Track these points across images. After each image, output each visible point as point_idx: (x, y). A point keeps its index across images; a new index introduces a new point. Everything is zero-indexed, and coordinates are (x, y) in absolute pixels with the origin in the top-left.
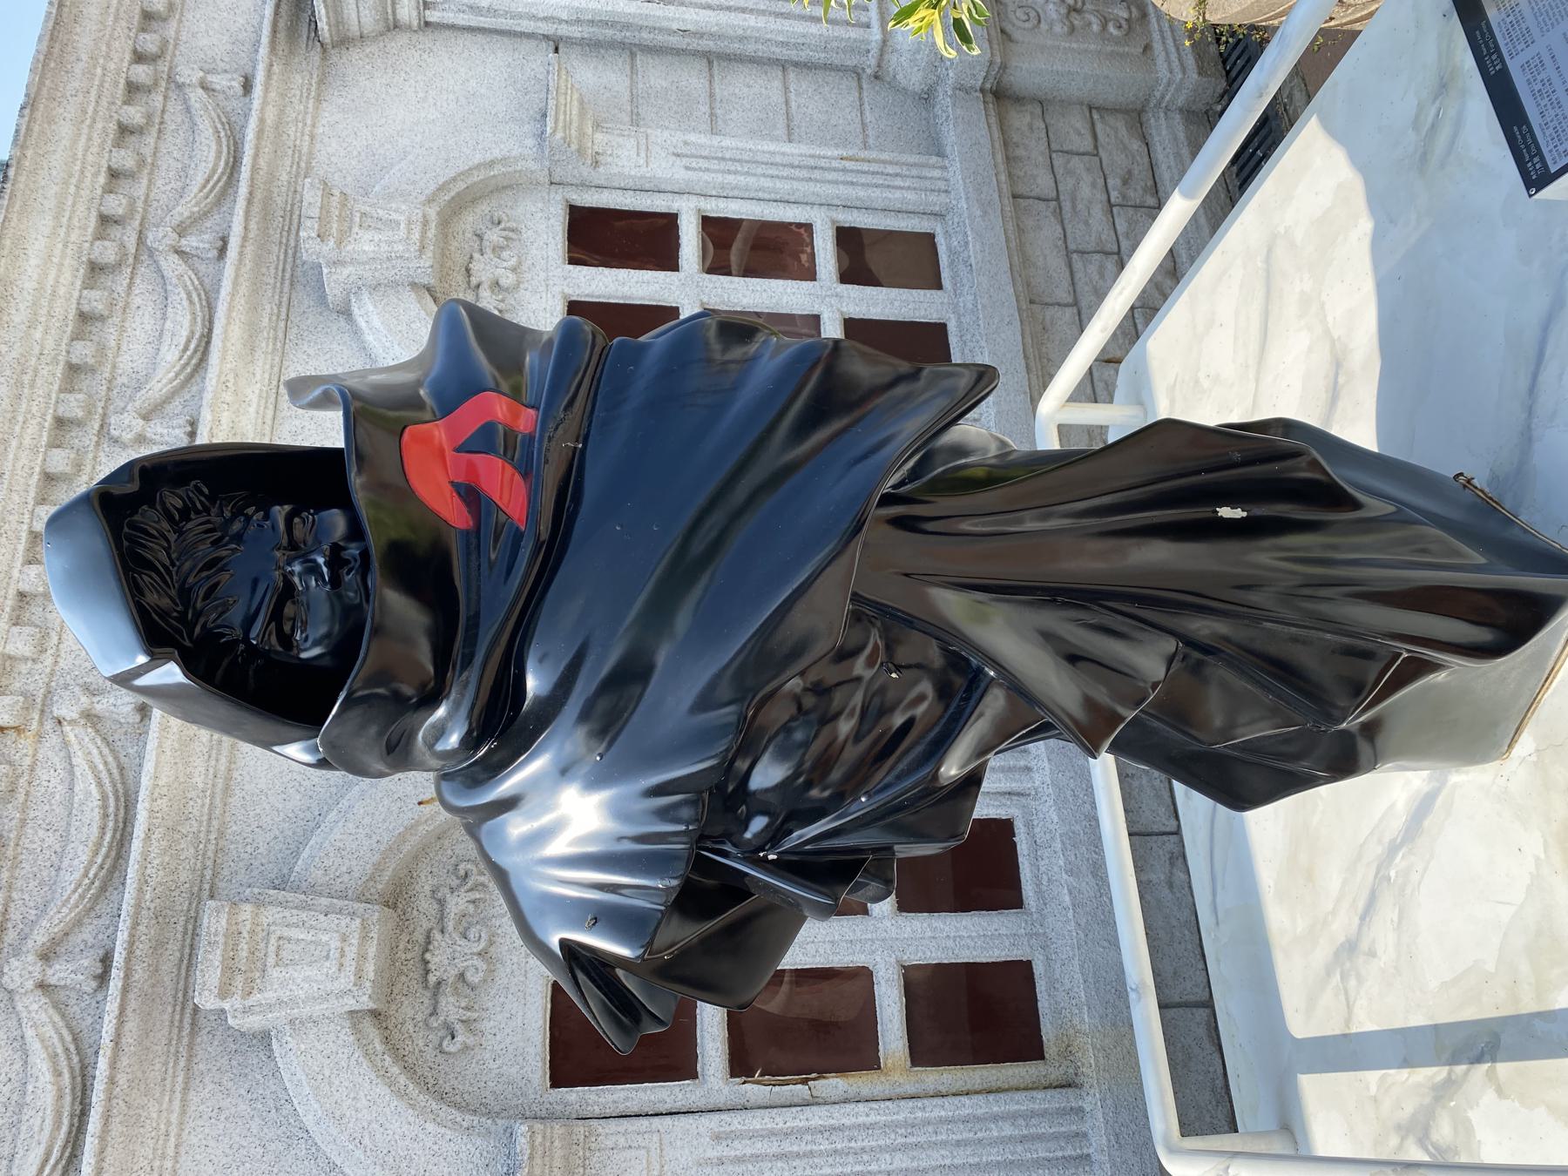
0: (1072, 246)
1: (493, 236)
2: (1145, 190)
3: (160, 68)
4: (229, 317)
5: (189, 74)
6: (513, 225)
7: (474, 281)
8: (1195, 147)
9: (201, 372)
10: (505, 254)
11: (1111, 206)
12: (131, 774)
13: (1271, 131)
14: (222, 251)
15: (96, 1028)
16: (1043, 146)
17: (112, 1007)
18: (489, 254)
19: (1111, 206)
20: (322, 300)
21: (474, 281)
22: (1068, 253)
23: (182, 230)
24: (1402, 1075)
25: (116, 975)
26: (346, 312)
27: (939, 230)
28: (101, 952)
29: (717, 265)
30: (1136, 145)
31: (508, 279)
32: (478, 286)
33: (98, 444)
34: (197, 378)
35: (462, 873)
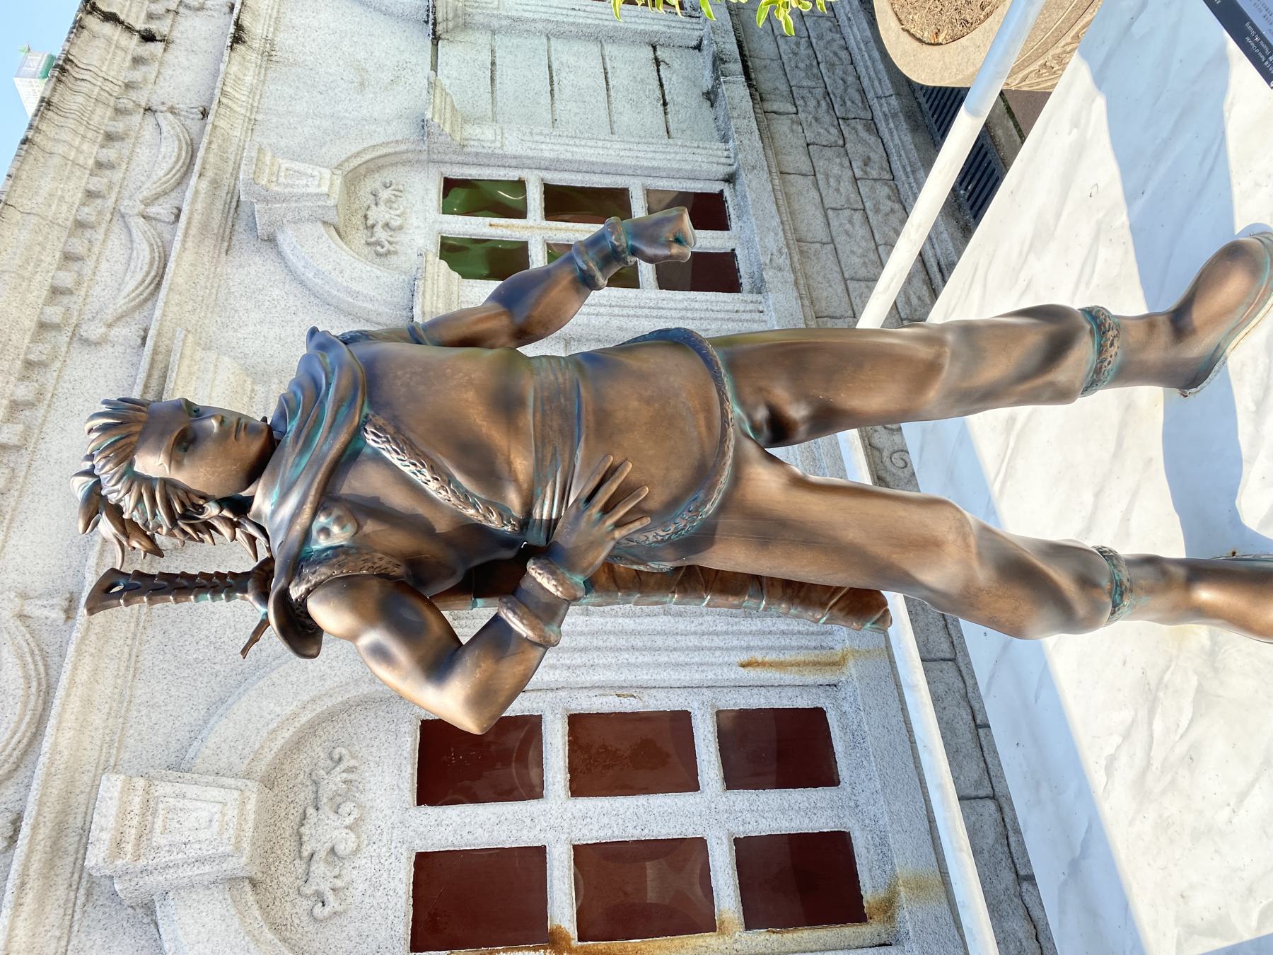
0: (847, 276)
1: (385, 194)
2: (882, 168)
3: (124, 151)
4: (184, 241)
5: (132, 206)
6: (401, 188)
7: (370, 222)
8: (928, 164)
9: (31, 757)
10: (395, 206)
11: (856, 180)
12: (52, 672)
13: (990, 163)
14: (178, 217)
15: (171, 242)
16: (839, 277)
17: (180, 233)
18: (326, 809)
19: (856, 180)
20: (253, 228)
21: (370, 222)
22: (825, 211)
23: (148, 202)
24: (972, 314)
25: (183, 218)
26: (271, 240)
27: (727, 194)
28: (11, 817)
29: (584, 781)
30: (873, 140)
31: (346, 841)
32: (373, 226)
33: (70, 344)
34: (150, 304)
35: (336, 757)
